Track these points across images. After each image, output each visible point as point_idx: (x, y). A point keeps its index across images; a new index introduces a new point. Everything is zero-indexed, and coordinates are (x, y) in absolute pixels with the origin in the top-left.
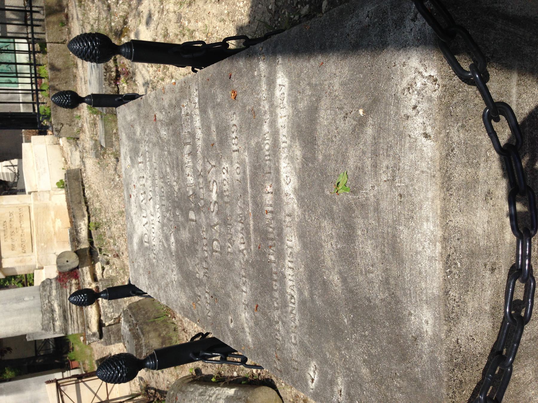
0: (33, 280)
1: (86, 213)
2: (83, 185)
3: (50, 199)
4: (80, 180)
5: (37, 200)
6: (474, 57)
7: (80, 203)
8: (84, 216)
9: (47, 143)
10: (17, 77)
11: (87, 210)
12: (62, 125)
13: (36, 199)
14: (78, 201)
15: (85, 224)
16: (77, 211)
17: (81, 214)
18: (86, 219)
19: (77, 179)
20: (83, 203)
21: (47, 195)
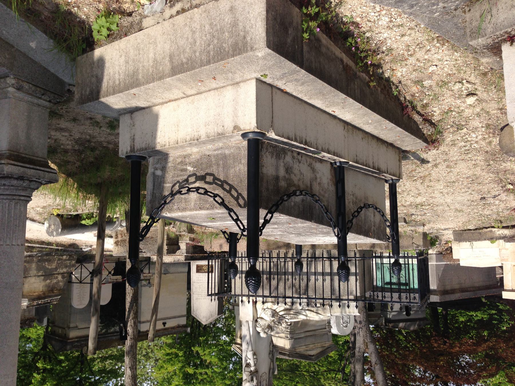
0: (18, 372)
1: (489, 229)
2: (465, 230)
3: (507, 249)
4: (461, 232)
5: (507, 259)
6: (54, 247)
7: (480, 233)
8: (491, 231)
9: (458, 248)
10: (408, 264)
11: (486, 228)
12: (413, 243)
13: (507, 260)
14: (479, 234)
15: (499, 231)
16: (487, 236)
17: (489, 233)
18: (493, 230)
19: (461, 235)
20: (481, 231)
21: (503, 251)
